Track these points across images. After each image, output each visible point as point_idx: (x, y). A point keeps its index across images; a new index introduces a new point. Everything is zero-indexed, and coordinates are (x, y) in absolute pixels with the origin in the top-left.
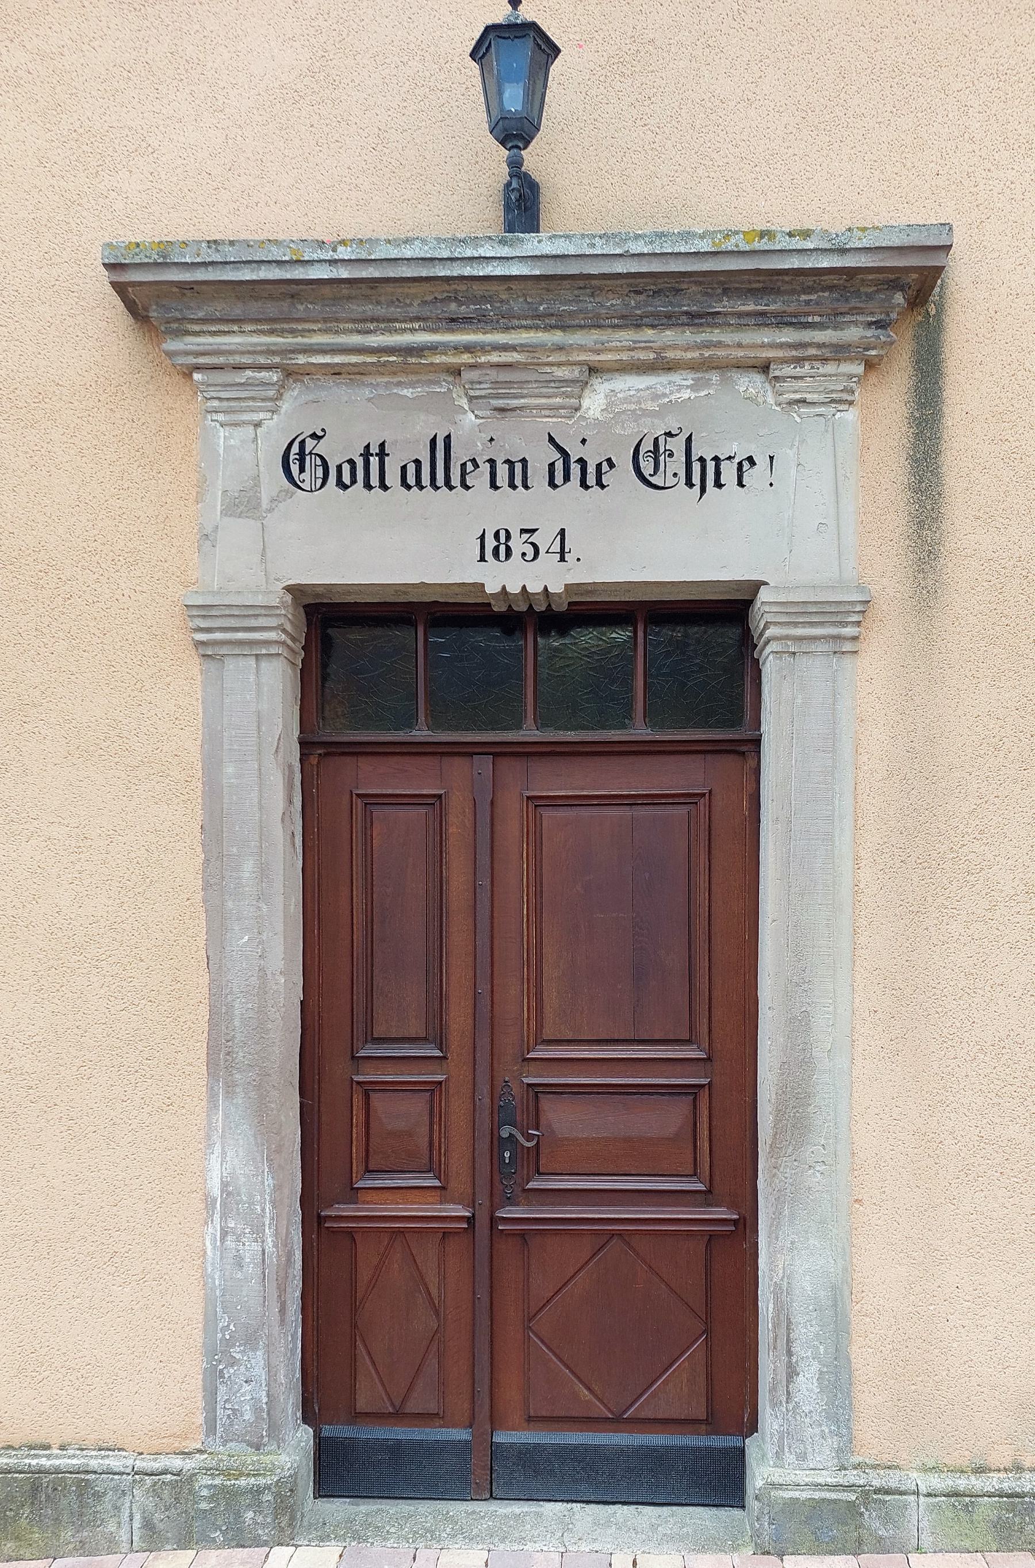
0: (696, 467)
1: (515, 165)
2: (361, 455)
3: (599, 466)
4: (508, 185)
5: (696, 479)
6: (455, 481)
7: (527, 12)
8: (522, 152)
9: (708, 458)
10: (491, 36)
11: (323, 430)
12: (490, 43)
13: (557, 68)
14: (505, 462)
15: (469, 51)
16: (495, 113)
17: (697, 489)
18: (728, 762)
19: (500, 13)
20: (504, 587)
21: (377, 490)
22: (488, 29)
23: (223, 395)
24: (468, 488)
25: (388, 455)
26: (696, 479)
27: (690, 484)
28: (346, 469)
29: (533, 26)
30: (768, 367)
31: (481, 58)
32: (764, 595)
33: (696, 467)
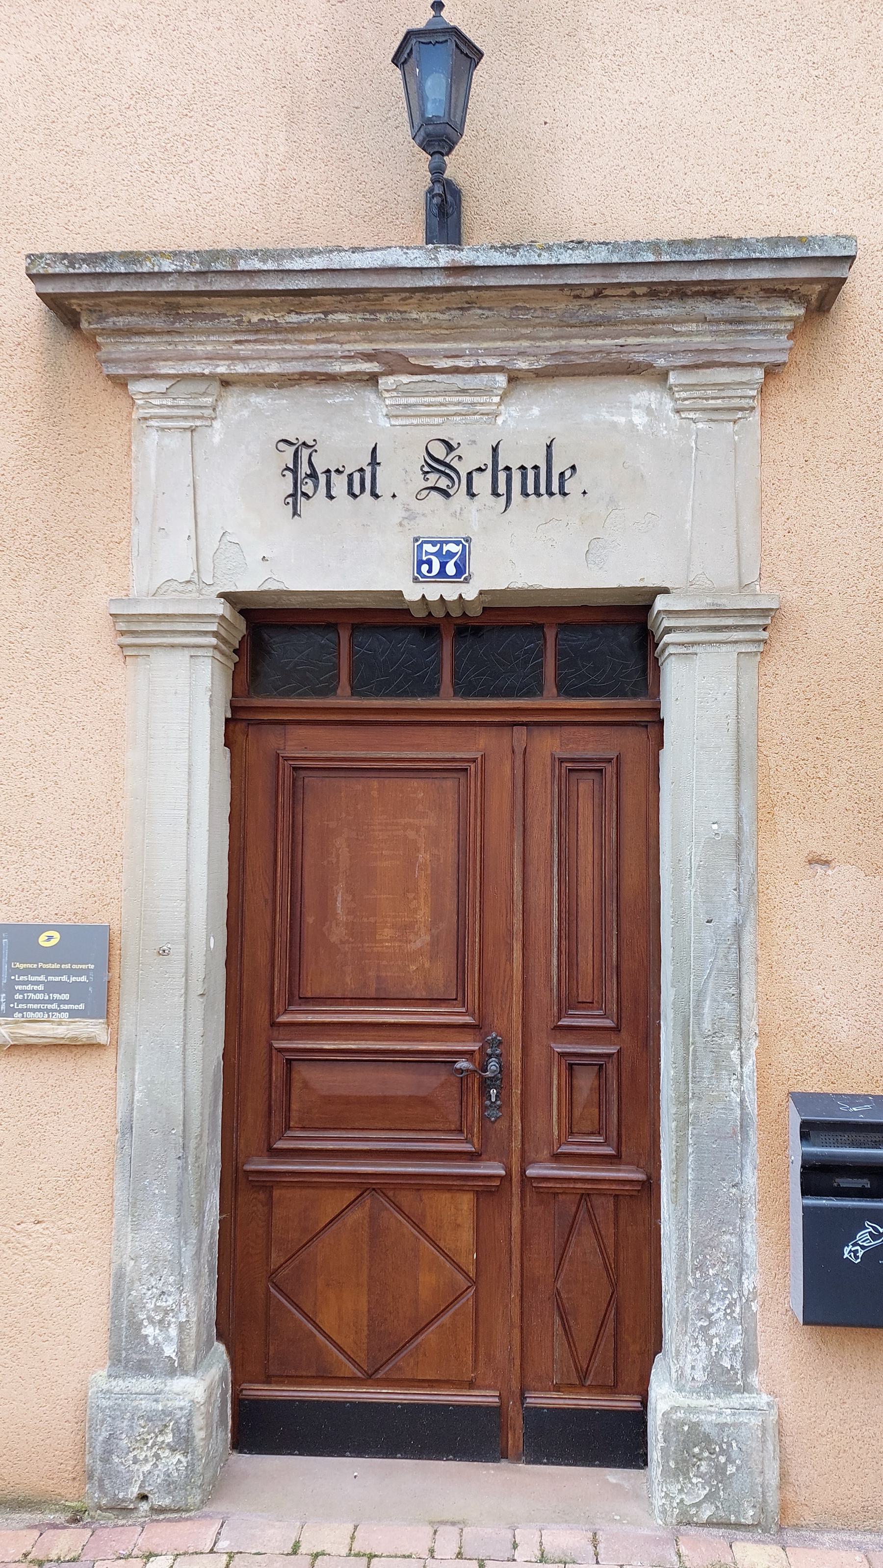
0: (502, 477)
1: (437, 171)
2: (369, 464)
3: (562, 474)
4: (430, 191)
5: (502, 489)
6: (555, 488)
7: (451, 16)
8: (445, 158)
9: (514, 467)
10: (413, 41)
11: (315, 440)
12: (412, 49)
13: (479, 74)
14: (519, 468)
15: (392, 56)
16: (417, 122)
17: (503, 499)
18: (463, 773)
19: (422, 18)
20: (423, 596)
21: (558, 497)
22: (409, 35)
23: (723, 394)
24: (565, 494)
25: (379, 464)
26: (502, 489)
27: (495, 493)
28: (357, 477)
29: (455, 32)
30: (667, 374)
31: (403, 63)
32: (660, 603)
33: (502, 477)
